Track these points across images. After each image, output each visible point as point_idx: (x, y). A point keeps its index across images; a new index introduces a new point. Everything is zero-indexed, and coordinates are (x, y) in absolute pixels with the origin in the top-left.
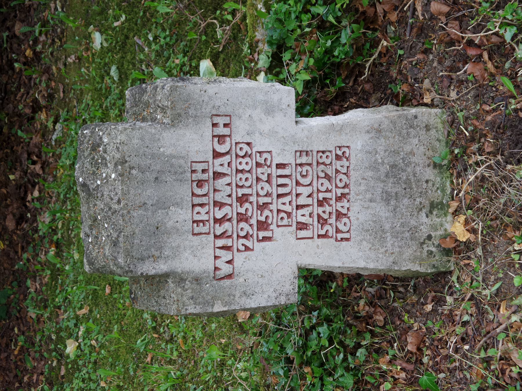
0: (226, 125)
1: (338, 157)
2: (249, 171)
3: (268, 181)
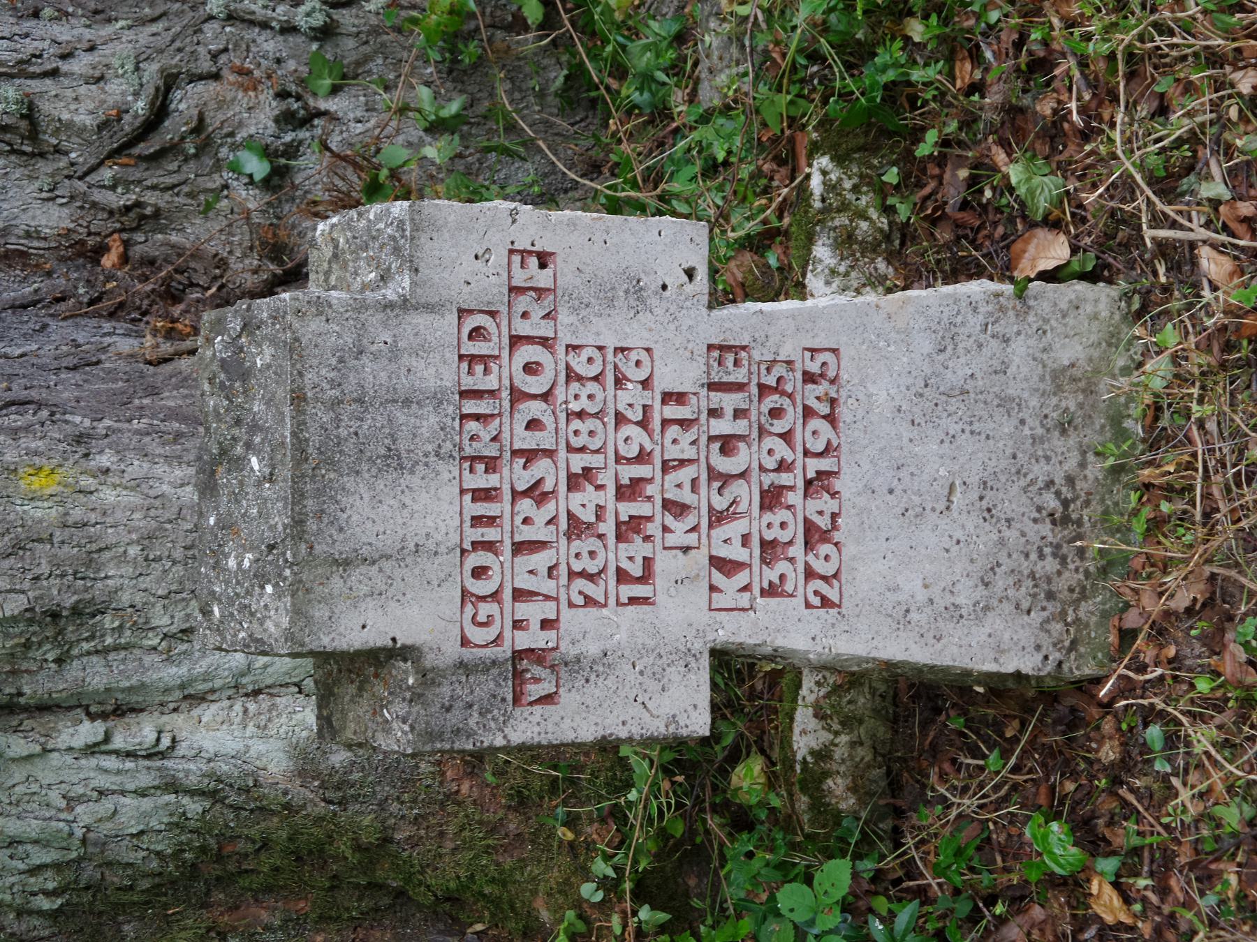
0: (546, 624)
1: (809, 378)
2: (596, 415)
3: (644, 424)
